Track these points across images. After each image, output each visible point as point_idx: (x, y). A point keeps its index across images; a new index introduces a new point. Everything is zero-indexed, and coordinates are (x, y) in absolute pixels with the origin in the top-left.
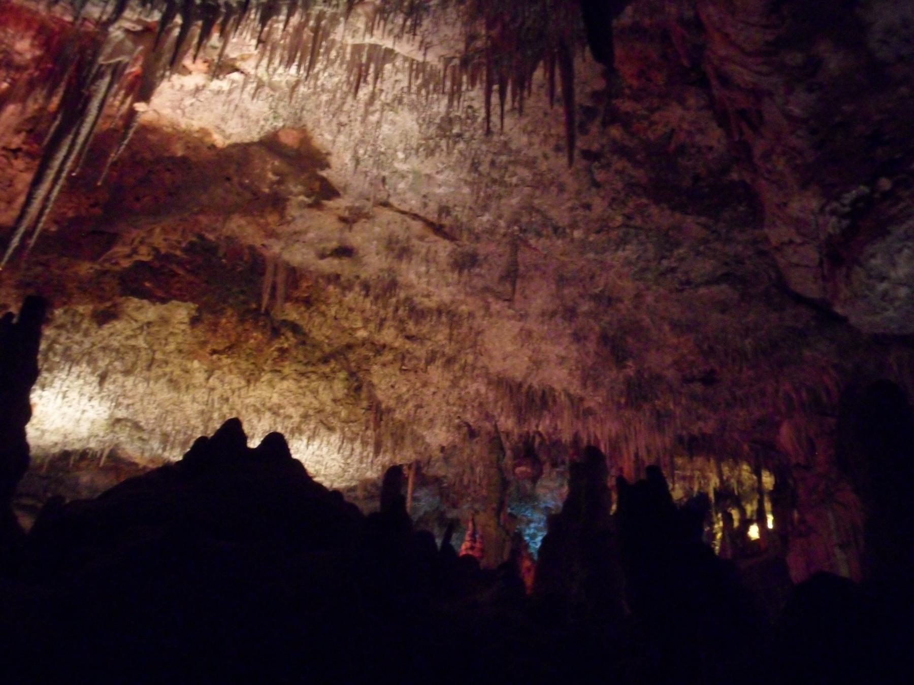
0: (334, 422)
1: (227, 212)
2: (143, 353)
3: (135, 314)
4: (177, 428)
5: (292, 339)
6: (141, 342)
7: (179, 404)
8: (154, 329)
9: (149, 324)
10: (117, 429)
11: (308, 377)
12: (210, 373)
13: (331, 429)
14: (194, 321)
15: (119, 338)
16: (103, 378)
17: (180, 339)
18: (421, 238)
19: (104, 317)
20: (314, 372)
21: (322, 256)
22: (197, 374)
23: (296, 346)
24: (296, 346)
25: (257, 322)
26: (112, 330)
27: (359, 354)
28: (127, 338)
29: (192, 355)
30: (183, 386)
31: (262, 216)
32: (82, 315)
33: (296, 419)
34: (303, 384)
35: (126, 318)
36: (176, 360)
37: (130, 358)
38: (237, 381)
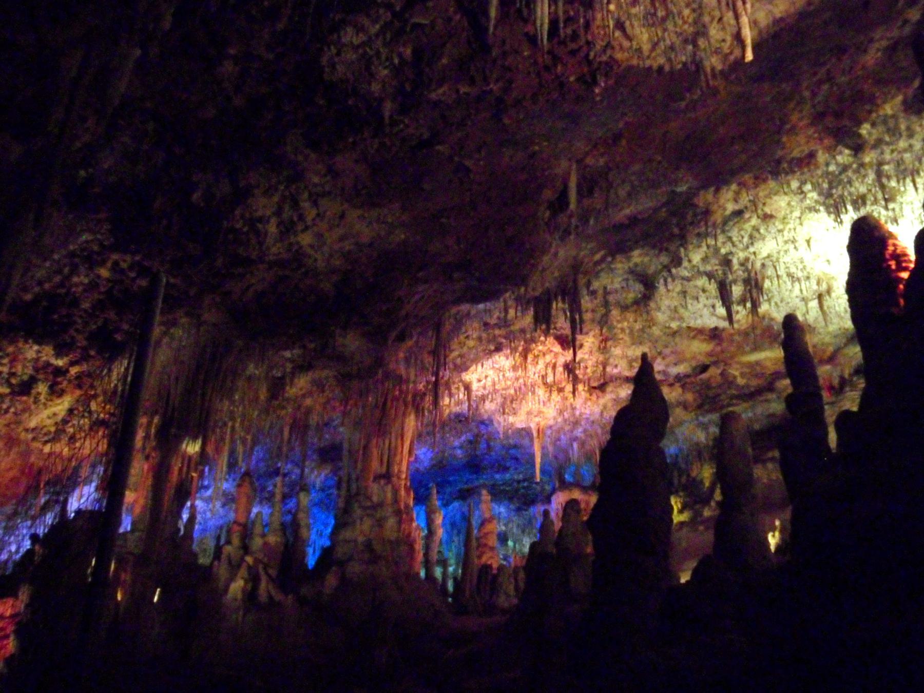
32: (893, 116)
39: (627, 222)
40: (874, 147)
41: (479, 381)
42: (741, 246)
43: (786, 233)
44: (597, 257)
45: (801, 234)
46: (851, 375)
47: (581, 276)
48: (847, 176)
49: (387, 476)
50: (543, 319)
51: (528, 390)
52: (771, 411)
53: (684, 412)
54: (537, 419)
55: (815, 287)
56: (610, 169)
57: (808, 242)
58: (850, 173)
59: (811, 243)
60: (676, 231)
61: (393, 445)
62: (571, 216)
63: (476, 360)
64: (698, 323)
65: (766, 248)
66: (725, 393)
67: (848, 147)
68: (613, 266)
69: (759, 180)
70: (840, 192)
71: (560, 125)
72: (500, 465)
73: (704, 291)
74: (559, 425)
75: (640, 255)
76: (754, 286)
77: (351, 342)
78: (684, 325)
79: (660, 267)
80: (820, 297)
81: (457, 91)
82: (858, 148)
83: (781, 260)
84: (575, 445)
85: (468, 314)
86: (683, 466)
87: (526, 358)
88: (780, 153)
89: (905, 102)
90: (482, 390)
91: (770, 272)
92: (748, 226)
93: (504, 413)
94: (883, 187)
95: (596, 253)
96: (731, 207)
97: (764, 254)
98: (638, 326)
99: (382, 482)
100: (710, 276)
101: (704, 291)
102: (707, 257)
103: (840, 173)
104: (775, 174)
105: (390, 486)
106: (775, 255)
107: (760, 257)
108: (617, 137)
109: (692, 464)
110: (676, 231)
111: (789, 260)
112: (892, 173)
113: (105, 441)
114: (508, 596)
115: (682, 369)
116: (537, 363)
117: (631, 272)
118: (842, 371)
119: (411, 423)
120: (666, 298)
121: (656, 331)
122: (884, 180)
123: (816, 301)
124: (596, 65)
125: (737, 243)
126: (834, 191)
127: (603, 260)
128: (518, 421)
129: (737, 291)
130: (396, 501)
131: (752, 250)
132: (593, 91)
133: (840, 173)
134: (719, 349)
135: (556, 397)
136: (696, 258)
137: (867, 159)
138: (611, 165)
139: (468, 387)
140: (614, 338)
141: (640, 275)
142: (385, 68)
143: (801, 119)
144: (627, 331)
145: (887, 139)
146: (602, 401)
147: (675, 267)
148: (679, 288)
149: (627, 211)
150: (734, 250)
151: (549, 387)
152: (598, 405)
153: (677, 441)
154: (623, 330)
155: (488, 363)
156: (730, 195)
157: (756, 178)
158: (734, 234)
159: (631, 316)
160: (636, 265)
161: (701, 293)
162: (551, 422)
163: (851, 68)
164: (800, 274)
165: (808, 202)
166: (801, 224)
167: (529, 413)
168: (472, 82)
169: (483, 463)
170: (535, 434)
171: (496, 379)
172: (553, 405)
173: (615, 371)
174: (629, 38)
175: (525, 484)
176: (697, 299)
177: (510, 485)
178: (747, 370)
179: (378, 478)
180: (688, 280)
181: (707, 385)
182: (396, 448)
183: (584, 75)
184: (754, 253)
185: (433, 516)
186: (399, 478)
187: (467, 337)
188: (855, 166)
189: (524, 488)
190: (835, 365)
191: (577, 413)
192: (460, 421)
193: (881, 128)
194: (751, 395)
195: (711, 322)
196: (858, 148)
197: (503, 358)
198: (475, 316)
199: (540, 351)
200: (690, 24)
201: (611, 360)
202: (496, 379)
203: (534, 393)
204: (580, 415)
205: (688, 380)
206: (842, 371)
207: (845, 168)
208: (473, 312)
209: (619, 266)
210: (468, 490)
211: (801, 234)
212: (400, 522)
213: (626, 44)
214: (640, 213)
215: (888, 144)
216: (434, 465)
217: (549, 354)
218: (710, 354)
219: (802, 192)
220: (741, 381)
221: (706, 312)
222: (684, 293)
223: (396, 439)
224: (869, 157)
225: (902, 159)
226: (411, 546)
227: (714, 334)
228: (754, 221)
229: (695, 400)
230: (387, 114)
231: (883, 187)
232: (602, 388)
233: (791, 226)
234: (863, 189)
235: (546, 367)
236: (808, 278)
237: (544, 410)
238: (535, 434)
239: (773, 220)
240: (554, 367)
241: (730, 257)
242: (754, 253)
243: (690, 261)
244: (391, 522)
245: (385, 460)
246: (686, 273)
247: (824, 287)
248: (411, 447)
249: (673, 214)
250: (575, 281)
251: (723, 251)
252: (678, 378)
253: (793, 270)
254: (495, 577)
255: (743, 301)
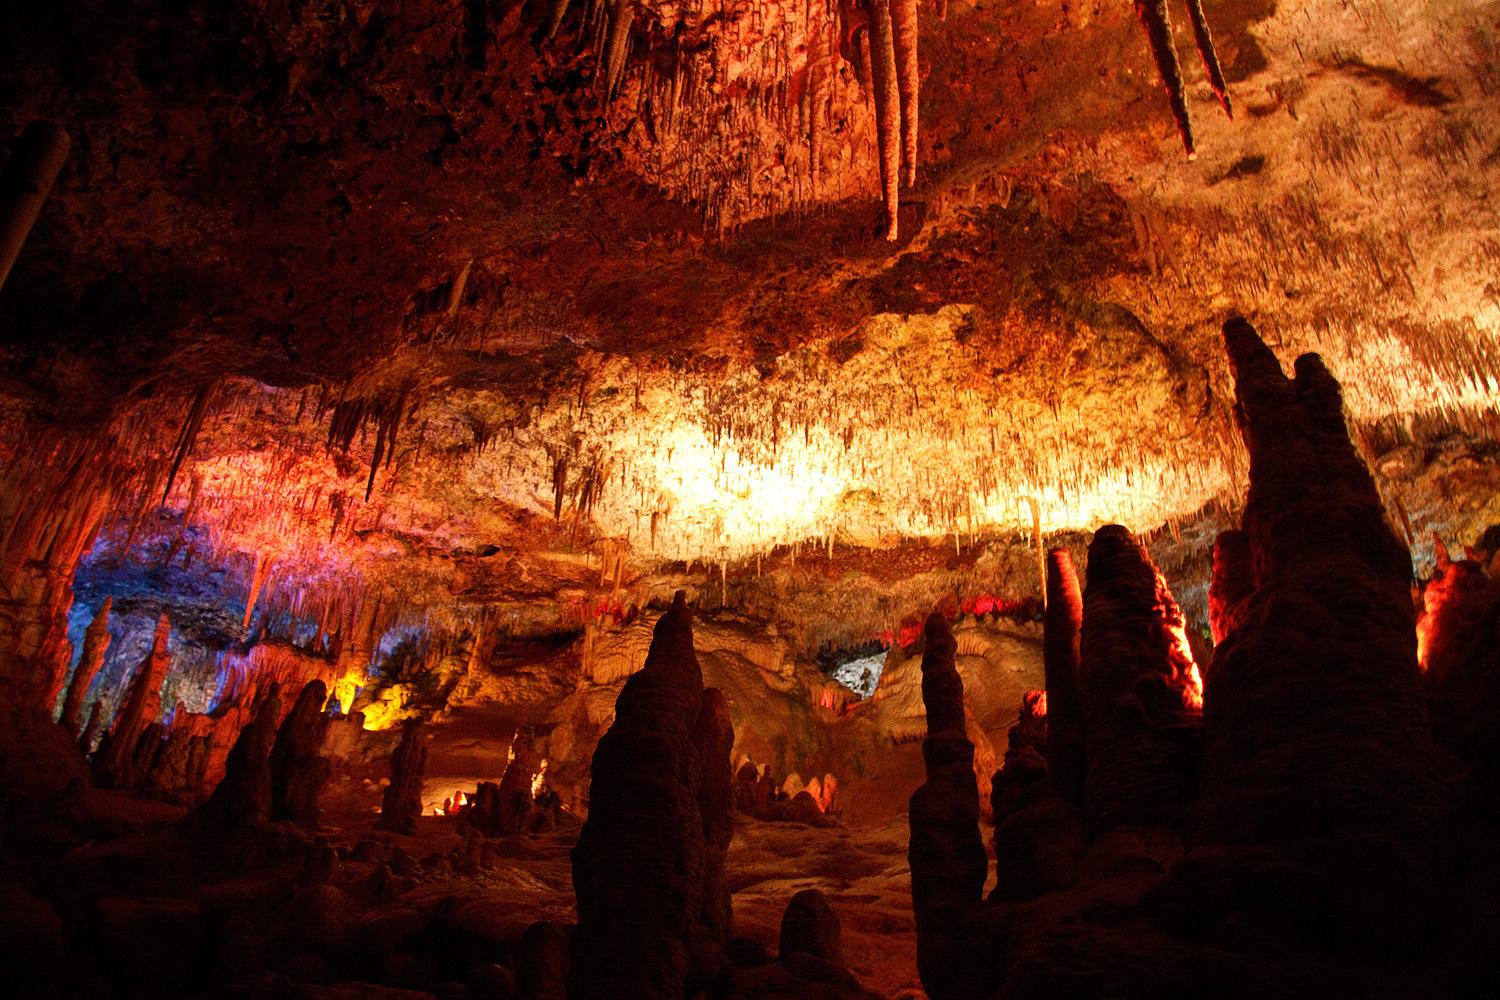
0: (1160, 441)
1: (1089, 130)
2: (899, 392)
3: (883, 340)
4: (942, 489)
5: (1090, 335)
6: (895, 378)
7: (944, 457)
8: (907, 357)
9: (901, 349)
10: (849, 505)
11: (1120, 385)
12: (991, 403)
13: (1158, 452)
14: (961, 335)
15: (866, 377)
16: (847, 438)
17: (945, 363)
18: (1378, 115)
19: (843, 352)
20: (1126, 377)
21: (1213, 180)
22: (973, 408)
23: (1098, 344)
24: (1098, 344)
25: (1049, 318)
26: (856, 368)
27: (1203, 336)
28: (876, 375)
29: (963, 382)
30: (957, 427)
31: (1144, 128)
32: (816, 354)
33: (1111, 446)
34: (1116, 395)
35: (872, 346)
36: (948, 392)
37: (883, 403)
38: (1028, 406)
39: (493, 353)
40: (784, 378)
41: (215, 478)
42: (599, 430)
43: (652, 433)
44: (438, 381)
45: (667, 441)
46: (644, 608)
47: (410, 397)
48: (744, 397)
49: (44, 566)
50: (343, 429)
51: (262, 501)
52: (540, 619)
53: (447, 593)
54: (268, 548)
55: (654, 502)
56: (509, 283)
57: (670, 452)
58: (748, 396)
59: (673, 454)
60: (541, 386)
61: (67, 525)
62: (439, 321)
63: (222, 453)
64: (509, 498)
65: (624, 441)
66: (502, 585)
67: (758, 368)
68: (448, 399)
69: (655, 365)
70: (729, 412)
71: (491, 204)
72: (190, 586)
73: (535, 464)
74: (292, 564)
75: (486, 397)
76: (593, 483)
77: (73, 373)
78: (492, 495)
79: (502, 420)
80: (655, 515)
81: (411, 97)
82: (766, 374)
83: (633, 461)
84: (302, 593)
85: (247, 391)
86: (419, 653)
87: (287, 470)
88: (697, 345)
89: (830, 345)
90: (214, 491)
91: (616, 469)
92: (615, 410)
93: (228, 528)
94: (776, 424)
95: (440, 376)
96: (611, 382)
97: (618, 448)
98: (439, 478)
99: (34, 572)
100: (551, 451)
101: (535, 464)
102: (556, 428)
103: (739, 391)
104: (676, 365)
105: (44, 580)
106: (629, 453)
107: (613, 449)
108: (538, 250)
109: (431, 653)
110: (541, 386)
111: (642, 462)
112: (790, 412)
113: (58, 676)
114: (175, 771)
115: (466, 544)
116: (299, 481)
117: (468, 413)
118: (637, 600)
119: (103, 503)
120: (487, 459)
121: (457, 491)
122: (779, 417)
123: (650, 517)
124: (593, 151)
125: (596, 424)
126: (724, 408)
127: (442, 387)
128: (244, 543)
129: (572, 476)
130: (46, 602)
131: (609, 438)
132: (573, 182)
133: (739, 391)
134: (518, 535)
135: (304, 529)
136: (545, 423)
137: (771, 389)
138: (511, 279)
139: (196, 482)
140: (405, 482)
141: (477, 421)
142: (321, 18)
143: (733, 317)
144: (424, 480)
145: (800, 375)
146: (358, 551)
147: (519, 426)
148: (505, 451)
149: (502, 342)
150: (588, 431)
151: (298, 510)
152: (351, 554)
153: (422, 621)
154: (419, 476)
155: (238, 461)
156: (617, 368)
157: (654, 362)
158: (597, 412)
159: (435, 463)
160: (476, 407)
161: (530, 466)
162: (285, 557)
163: (806, 286)
164: (647, 484)
165: (691, 408)
166: (671, 430)
167: (260, 537)
168: (437, 94)
169: (176, 581)
170: (258, 565)
171: (238, 483)
172: (296, 537)
173: (391, 521)
174: (654, 139)
175: (209, 615)
176: (524, 471)
177: (190, 611)
178: (537, 568)
179: (31, 563)
180: (522, 445)
181: (487, 571)
182: (70, 529)
183: (570, 156)
184: (610, 443)
185: (96, 639)
186: (60, 573)
187: (227, 420)
188: (756, 390)
189: (205, 619)
190: (632, 592)
191: (322, 556)
192: (163, 518)
193: (799, 362)
194: (527, 596)
195: (524, 501)
196: (766, 374)
197: (259, 460)
198: (253, 397)
199: (307, 467)
200: (732, 158)
201: (391, 508)
202: (238, 483)
203: (278, 516)
204: (324, 560)
205: (467, 558)
206: (637, 600)
207: (745, 389)
208: (253, 392)
209: (456, 401)
210: (130, 603)
211: (667, 441)
212: (43, 635)
213: (646, 144)
214: (513, 349)
215: (798, 381)
216: (102, 563)
217: (321, 474)
218: (506, 538)
219: (689, 396)
220: (525, 578)
221: (523, 488)
222: (510, 459)
223: (74, 520)
224: (774, 387)
225: (805, 403)
226: (50, 678)
227: (522, 517)
228: (625, 407)
229: (465, 584)
230: (294, 82)
231: (776, 424)
232: (363, 536)
233: (661, 428)
234: (754, 418)
235: (308, 489)
236: (653, 491)
237: (283, 540)
238: (258, 565)
239: (644, 414)
240: (318, 492)
241: (581, 438)
242: (610, 443)
243: (536, 425)
244: (32, 632)
245: (49, 540)
246: (525, 438)
247: (664, 506)
248: (93, 533)
249: (547, 364)
250: (401, 402)
251: (576, 428)
252: (457, 552)
253: (641, 477)
254: (163, 747)
255: (574, 491)
